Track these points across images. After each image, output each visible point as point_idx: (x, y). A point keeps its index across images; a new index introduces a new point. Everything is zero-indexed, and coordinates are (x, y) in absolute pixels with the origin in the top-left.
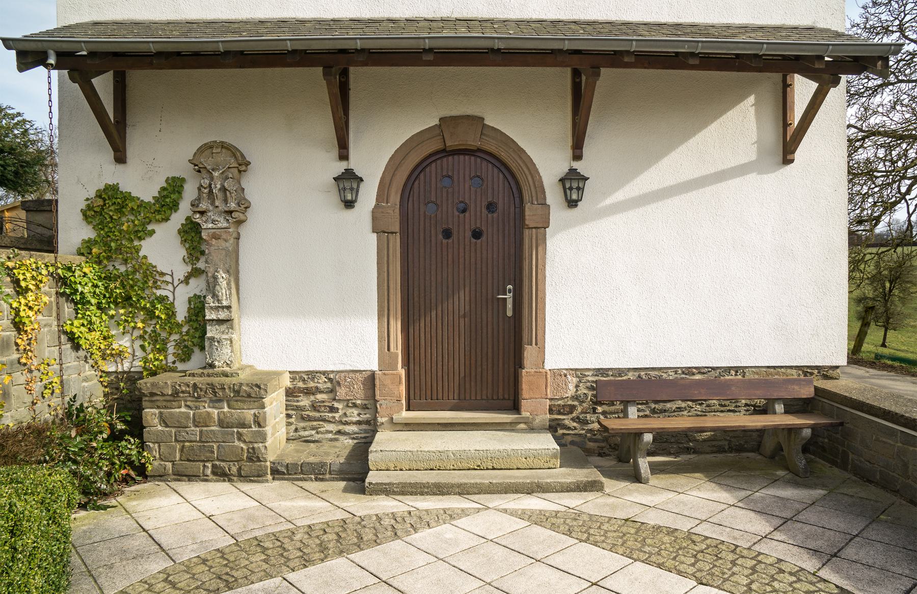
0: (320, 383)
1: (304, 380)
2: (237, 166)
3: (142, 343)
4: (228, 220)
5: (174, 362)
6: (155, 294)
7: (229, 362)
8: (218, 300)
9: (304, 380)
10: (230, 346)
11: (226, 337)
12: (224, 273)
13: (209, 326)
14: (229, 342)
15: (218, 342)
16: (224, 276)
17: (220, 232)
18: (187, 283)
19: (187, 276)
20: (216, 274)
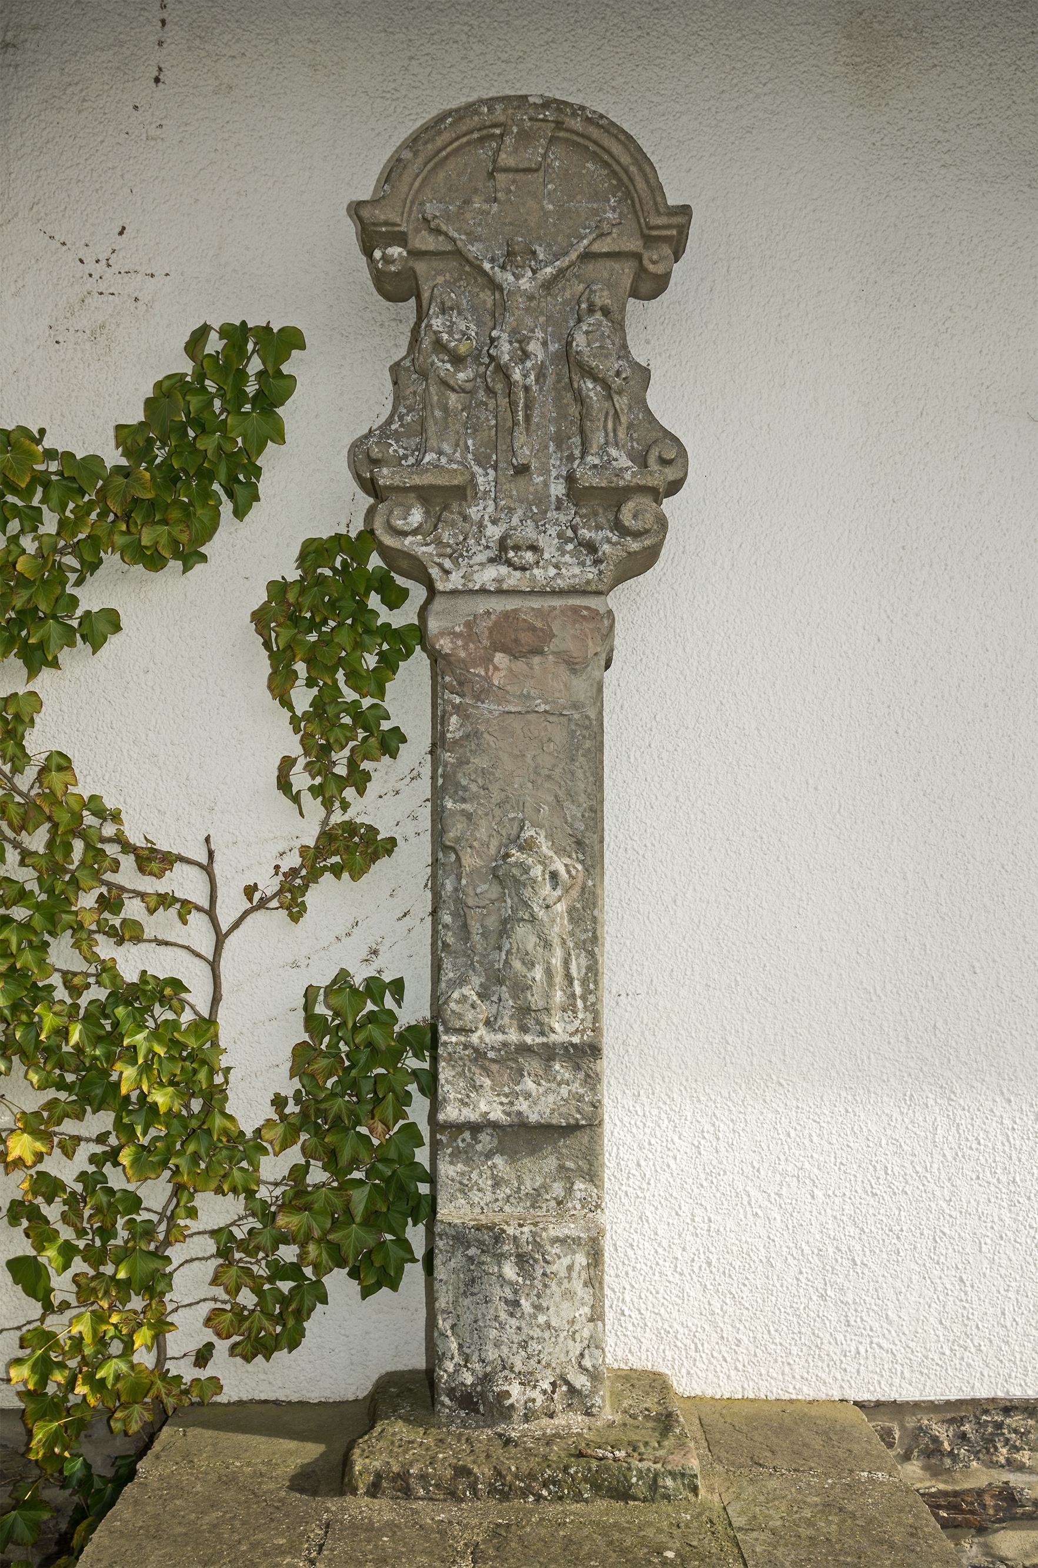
0: (1021, 1468)
1: (932, 1452)
2: (634, 245)
3: (24, 1248)
4: (591, 547)
5: (203, 1356)
6: (107, 970)
7: (580, 1381)
8: (524, 1013)
9: (932, 1452)
10: (589, 1283)
11: (570, 1229)
12: (561, 851)
13: (455, 1157)
14: (581, 1259)
15: (523, 1260)
16: (559, 865)
17: (539, 613)
18: (296, 911)
19: (294, 872)
20: (516, 855)
